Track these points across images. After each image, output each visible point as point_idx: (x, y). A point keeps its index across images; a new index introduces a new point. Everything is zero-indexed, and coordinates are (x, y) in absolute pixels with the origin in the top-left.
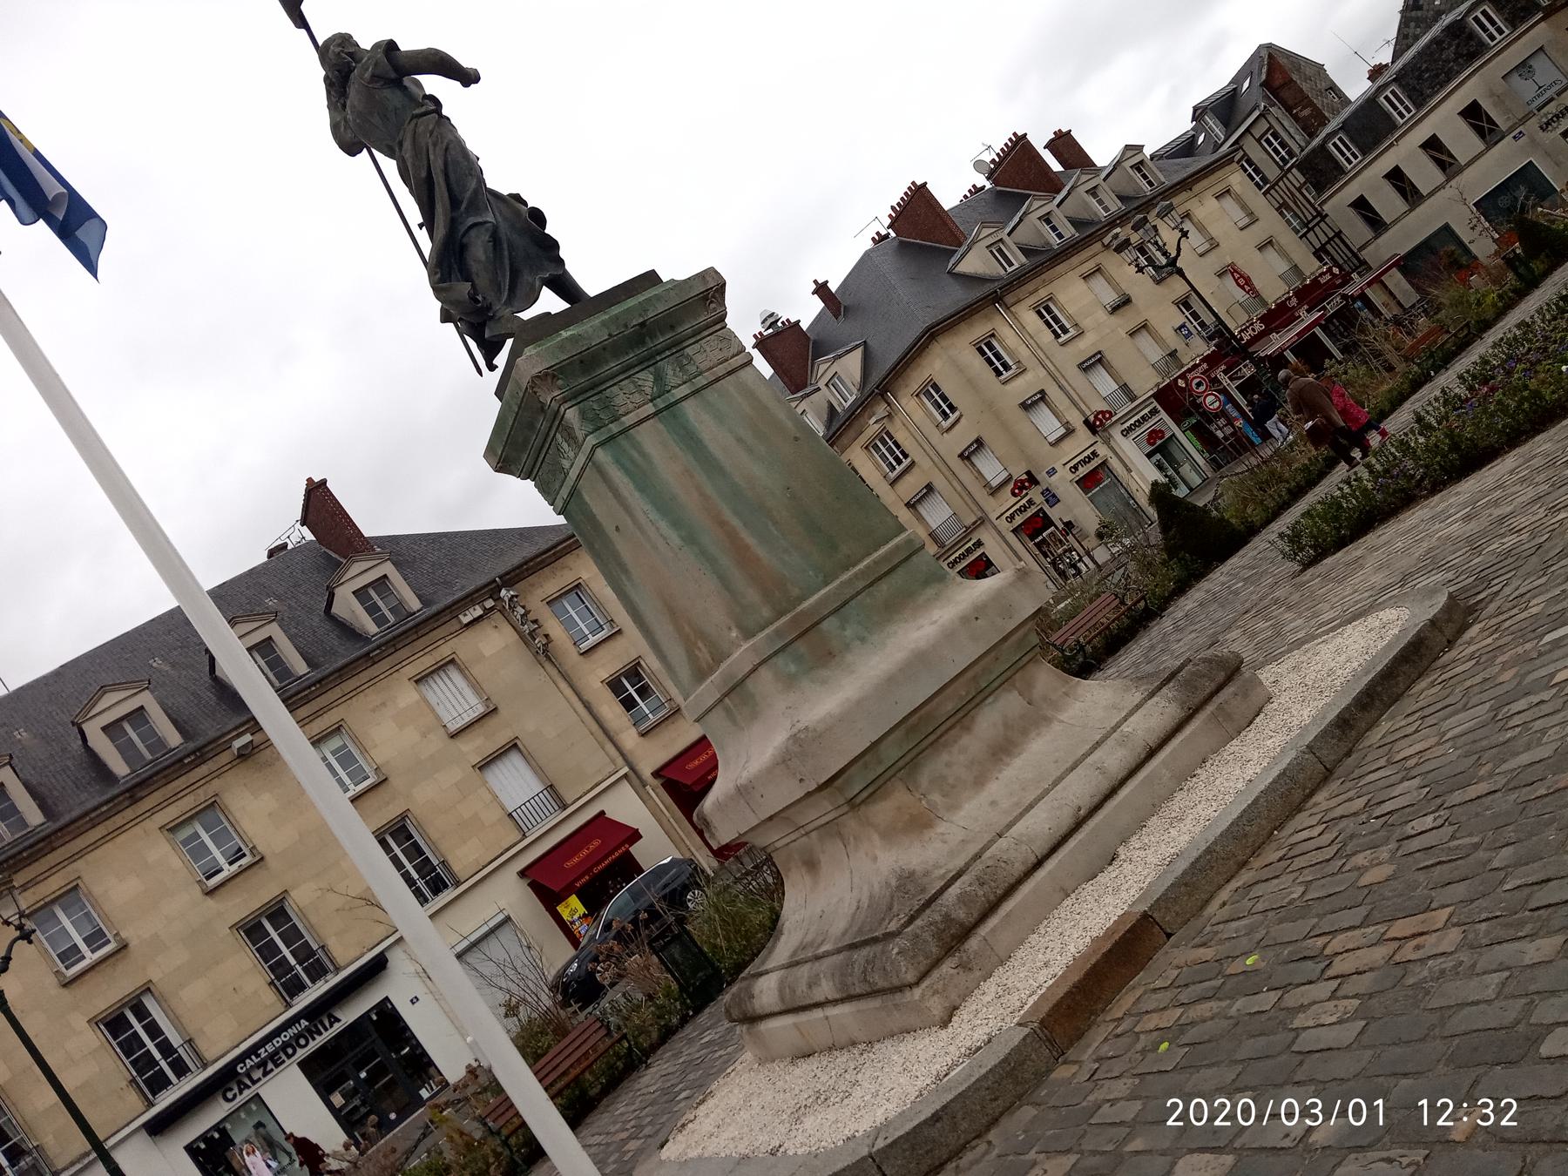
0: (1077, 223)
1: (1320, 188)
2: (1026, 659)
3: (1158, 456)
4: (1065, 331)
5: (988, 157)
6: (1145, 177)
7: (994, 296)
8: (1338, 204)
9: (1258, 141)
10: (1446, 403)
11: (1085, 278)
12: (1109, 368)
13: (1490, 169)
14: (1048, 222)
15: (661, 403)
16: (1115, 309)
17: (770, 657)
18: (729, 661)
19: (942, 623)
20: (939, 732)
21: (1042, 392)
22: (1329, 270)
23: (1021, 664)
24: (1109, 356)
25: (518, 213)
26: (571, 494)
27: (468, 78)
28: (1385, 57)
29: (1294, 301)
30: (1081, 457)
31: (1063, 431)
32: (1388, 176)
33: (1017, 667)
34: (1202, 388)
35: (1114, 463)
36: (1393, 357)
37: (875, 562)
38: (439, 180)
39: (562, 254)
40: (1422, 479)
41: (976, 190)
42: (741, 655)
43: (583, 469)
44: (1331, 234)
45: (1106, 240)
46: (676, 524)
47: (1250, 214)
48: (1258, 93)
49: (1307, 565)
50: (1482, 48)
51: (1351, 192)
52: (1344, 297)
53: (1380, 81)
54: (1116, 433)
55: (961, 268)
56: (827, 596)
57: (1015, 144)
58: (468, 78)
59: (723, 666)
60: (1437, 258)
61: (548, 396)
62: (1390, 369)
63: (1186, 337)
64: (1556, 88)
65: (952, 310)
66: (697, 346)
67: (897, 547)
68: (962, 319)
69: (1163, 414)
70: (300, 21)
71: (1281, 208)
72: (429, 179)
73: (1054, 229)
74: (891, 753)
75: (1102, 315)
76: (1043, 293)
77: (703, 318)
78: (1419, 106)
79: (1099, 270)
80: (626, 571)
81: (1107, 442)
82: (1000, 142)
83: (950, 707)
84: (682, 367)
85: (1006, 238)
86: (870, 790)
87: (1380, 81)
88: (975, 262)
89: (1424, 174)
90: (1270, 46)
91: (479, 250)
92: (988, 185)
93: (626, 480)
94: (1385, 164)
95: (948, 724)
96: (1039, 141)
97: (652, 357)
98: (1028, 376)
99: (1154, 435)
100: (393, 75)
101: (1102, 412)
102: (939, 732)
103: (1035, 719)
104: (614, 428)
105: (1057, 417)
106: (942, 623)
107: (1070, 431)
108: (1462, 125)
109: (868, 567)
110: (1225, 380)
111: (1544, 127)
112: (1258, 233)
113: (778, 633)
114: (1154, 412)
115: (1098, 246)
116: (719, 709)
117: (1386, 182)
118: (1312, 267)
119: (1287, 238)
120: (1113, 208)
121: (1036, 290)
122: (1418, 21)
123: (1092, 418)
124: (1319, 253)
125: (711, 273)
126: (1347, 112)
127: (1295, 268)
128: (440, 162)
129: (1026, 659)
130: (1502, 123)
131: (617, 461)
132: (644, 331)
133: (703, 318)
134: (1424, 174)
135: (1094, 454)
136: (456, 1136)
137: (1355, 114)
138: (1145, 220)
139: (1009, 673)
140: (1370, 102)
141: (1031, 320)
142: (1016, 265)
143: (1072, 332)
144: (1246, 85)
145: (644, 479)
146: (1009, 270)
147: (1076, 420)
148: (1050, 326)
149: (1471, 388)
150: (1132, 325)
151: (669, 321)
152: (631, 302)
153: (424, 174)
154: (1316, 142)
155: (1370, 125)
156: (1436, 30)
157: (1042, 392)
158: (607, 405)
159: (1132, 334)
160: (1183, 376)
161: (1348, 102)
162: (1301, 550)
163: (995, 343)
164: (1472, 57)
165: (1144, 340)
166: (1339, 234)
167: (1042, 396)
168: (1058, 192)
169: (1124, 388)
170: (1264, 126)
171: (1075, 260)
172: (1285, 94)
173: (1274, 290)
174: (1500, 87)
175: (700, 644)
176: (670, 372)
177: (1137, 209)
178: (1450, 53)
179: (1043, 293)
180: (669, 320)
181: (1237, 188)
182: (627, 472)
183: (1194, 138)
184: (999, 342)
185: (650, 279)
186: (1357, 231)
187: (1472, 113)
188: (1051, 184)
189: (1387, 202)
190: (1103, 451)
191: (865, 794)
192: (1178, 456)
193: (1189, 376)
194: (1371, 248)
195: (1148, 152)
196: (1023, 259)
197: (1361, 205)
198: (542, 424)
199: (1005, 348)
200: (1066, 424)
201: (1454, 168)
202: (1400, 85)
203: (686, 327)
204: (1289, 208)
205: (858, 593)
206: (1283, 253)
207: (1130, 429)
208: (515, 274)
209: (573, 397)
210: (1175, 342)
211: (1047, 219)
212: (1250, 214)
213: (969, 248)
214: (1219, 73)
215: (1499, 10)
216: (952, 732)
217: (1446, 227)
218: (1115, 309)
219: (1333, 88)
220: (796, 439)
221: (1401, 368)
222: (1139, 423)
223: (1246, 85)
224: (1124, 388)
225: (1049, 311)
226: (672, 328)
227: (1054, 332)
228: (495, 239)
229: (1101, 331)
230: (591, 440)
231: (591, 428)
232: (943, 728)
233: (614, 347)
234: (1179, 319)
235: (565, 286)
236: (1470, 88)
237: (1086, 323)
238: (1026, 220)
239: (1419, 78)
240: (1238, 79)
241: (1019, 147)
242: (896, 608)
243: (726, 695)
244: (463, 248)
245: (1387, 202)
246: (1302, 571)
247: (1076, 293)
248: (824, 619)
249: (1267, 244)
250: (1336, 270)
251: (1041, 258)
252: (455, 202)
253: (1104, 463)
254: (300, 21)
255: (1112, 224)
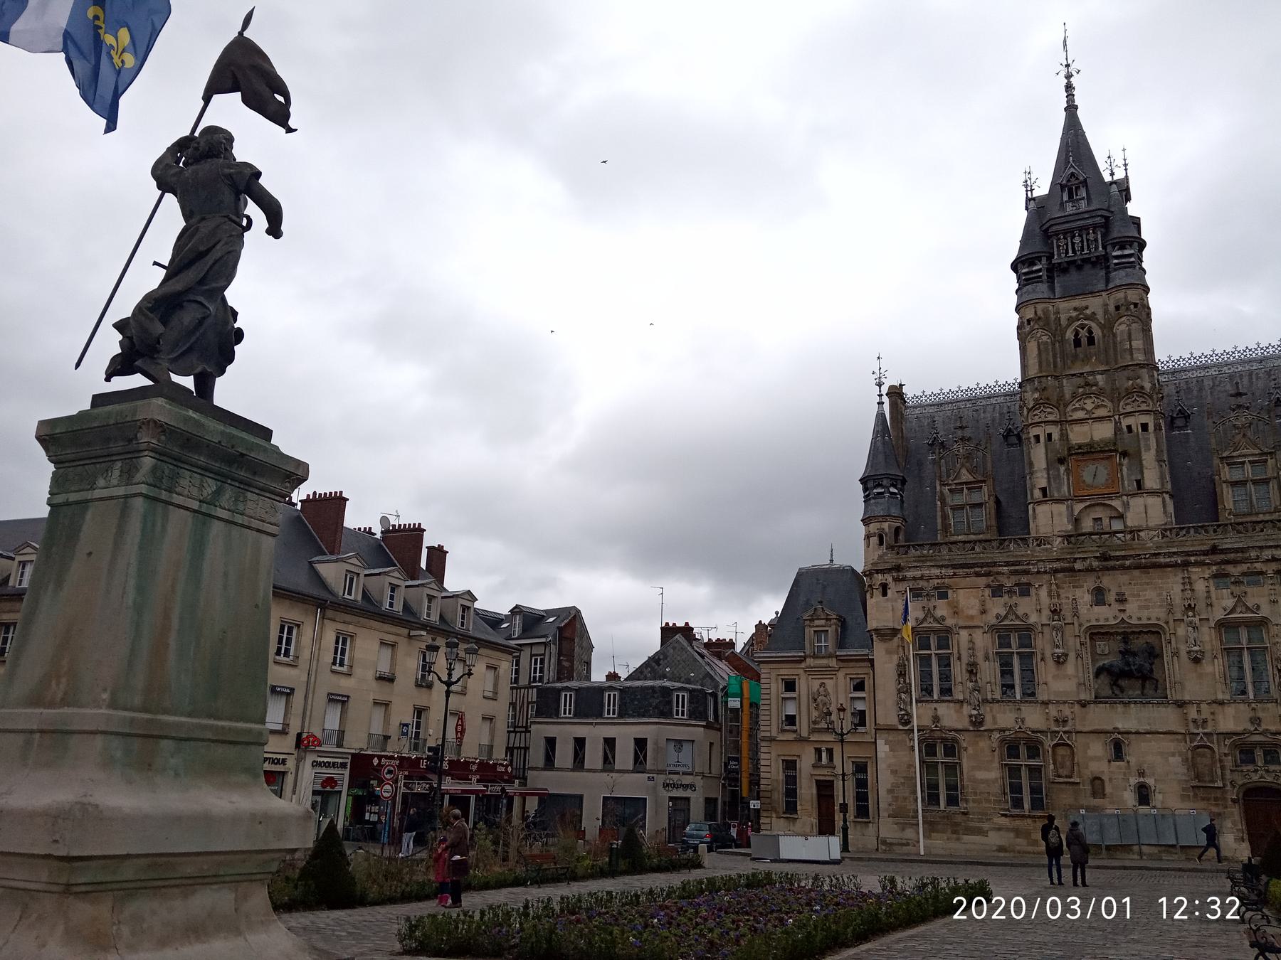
0: (406, 607)
1: (539, 714)
2: (258, 877)
3: (319, 798)
4: (341, 664)
5: (394, 521)
6: (463, 617)
7: (324, 603)
8: (542, 730)
9: (532, 656)
10: (545, 908)
11: (383, 643)
12: (344, 713)
13: (630, 785)
14: (393, 590)
15: (204, 508)
16: (381, 678)
17: (112, 733)
18: (75, 710)
19: (232, 804)
20: (167, 883)
21: (292, 690)
22: (506, 766)
23: (253, 877)
24: (351, 703)
25: (226, 323)
26: (77, 503)
27: (275, 230)
28: (623, 674)
29: (474, 768)
30: (274, 756)
31: (279, 727)
32: (576, 739)
33: (249, 878)
34: (388, 776)
35: (289, 779)
36: (512, 854)
37: (230, 729)
38: (209, 260)
39: (229, 368)
40: (515, 946)
41: (369, 532)
42: (94, 714)
43: (118, 497)
44: (523, 745)
45: (413, 633)
46: (140, 590)
47: (496, 693)
48: (553, 630)
49: (406, 952)
50: (668, 714)
51: (552, 730)
52: (503, 790)
53: (613, 684)
54: (310, 758)
55: (320, 567)
56: (181, 725)
57: (415, 529)
58: (275, 230)
59: (66, 710)
60: (561, 809)
61: (145, 438)
62: (505, 859)
63: (403, 734)
64: (684, 769)
65: (291, 587)
66: (256, 497)
67: (250, 731)
68: (290, 598)
69: (347, 772)
70: (207, 99)
71: (512, 704)
72: (201, 255)
73: (392, 597)
74: (127, 872)
75: (370, 675)
76: (351, 629)
77: (275, 485)
78: (620, 716)
79: (393, 646)
80: (59, 584)
81: (299, 760)
82: (407, 519)
83: (189, 870)
84: (236, 500)
85: (362, 576)
86: (89, 888)
87: (613, 684)
88: (331, 572)
89: (594, 756)
90: (578, 612)
91: (188, 316)
92: (378, 536)
93: (139, 533)
94: (581, 731)
95: (178, 882)
96: (429, 541)
97: (227, 477)
98: (293, 672)
99: (330, 781)
100: (241, 188)
101: (313, 736)
102: (167, 883)
103: (231, 926)
104: (164, 495)
105: (285, 715)
106: (232, 804)
107: (283, 732)
108: (631, 746)
109: (223, 728)
110: (401, 783)
111: (666, 785)
112: (490, 708)
113: (132, 720)
114: (343, 765)
115: (405, 631)
116: (20, 739)
117: (573, 742)
118: (499, 754)
119: (502, 725)
120: (432, 618)
121: (349, 623)
122: (653, 670)
123: (305, 736)
124: (510, 750)
125: (304, 467)
126: (584, 684)
127: (491, 747)
128: (219, 255)
129: (258, 877)
130: (649, 764)
131: (145, 517)
132: (239, 460)
133: (275, 485)
134: (594, 756)
135: (284, 761)
136: (952, 881)
137: (588, 688)
138: (456, 645)
139: (238, 878)
140: (599, 690)
141: (329, 638)
142: (352, 598)
143: (345, 669)
144: (551, 620)
145: (149, 541)
146: (346, 596)
147: (294, 729)
148: (336, 653)
149: (562, 910)
150: (380, 697)
151: (258, 468)
152: (244, 435)
153: (202, 248)
154: (558, 685)
155: (590, 703)
156: (658, 683)
157: (292, 690)
158: (174, 478)
159: (376, 703)
160: (380, 757)
161: (588, 678)
162: (410, 937)
163: (295, 632)
164: (663, 714)
165: (379, 713)
166: (526, 749)
167: (290, 693)
168: (413, 579)
169: (341, 733)
170: (541, 650)
171: (387, 627)
172: (565, 644)
173: (470, 751)
174: (663, 743)
175: (64, 680)
176: (227, 496)
177: (442, 629)
178: (655, 702)
179: (351, 629)
180: (249, 461)
181: (501, 671)
182: (144, 530)
183: (501, 621)
184: (298, 634)
185: (266, 433)
186: (536, 756)
187: (641, 744)
188: (412, 571)
189: (564, 754)
190: (291, 763)
191: (83, 889)
192: (331, 807)
193: (383, 761)
194: (535, 773)
195: (477, 605)
196: (359, 598)
197: (551, 742)
198: (117, 446)
199: (297, 641)
200: (286, 725)
201: (608, 767)
202: (621, 699)
203: (262, 481)
204: (514, 709)
205: (203, 740)
206: (492, 732)
207: (319, 764)
208: (190, 350)
209: (160, 454)
210: (394, 731)
211: (394, 588)
212: (496, 693)
213: (336, 561)
214: (542, 601)
215: (690, 702)
216: (176, 891)
217: (581, 797)
218: (381, 678)
219: (588, 664)
220: (257, 606)
221: (511, 863)
222: (328, 765)
223: (551, 620)
224: (341, 733)
225: (344, 643)
226: (255, 474)
227: (335, 659)
228: (201, 322)
229: (360, 685)
230: (143, 489)
231: (151, 480)
232: (172, 882)
233: (214, 451)
234: (408, 718)
235: (205, 385)
236: (648, 730)
237: (358, 671)
238: (419, 589)
239: (632, 700)
240: (550, 612)
241: (416, 533)
242: (216, 772)
243: (42, 732)
244: (181, 307)
245: (564, 754)
246: (402, 954)
247: (369, 648)
248: (166, 737)
249: (488, 719)
250: (509, 769)
251: (371, 608)
252: (202, 282)
253: (284, 773)
254: (207, 99)
255: (424, 626)
